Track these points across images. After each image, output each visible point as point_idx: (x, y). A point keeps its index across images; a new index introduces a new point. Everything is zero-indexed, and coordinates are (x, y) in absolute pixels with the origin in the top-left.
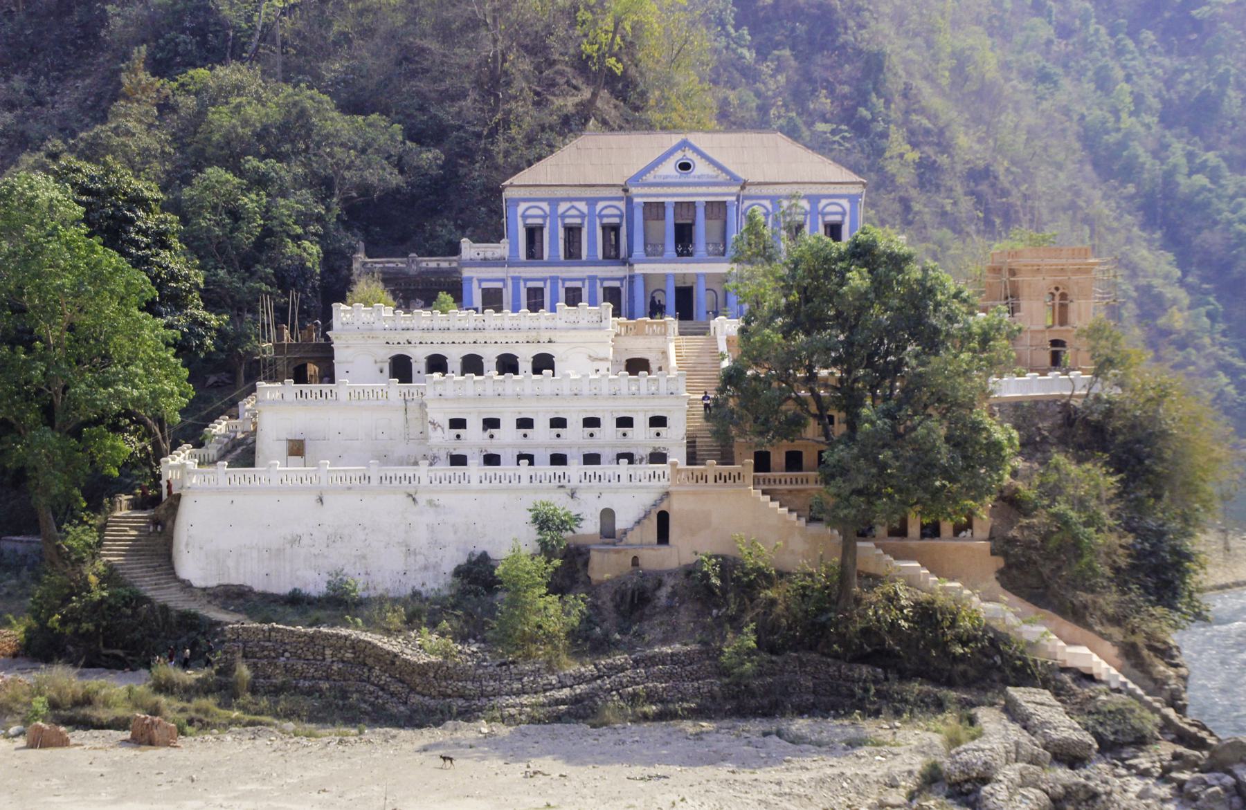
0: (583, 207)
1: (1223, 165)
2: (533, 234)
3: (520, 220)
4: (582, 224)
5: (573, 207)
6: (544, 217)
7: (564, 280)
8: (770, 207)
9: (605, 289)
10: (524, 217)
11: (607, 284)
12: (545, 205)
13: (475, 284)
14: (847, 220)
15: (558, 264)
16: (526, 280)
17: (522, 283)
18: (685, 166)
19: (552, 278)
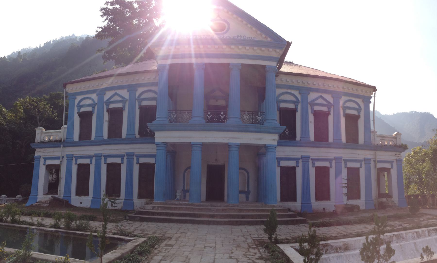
2: (86, 117)
4: (124, 107)
5: (321, 97)
6: (93, 105)
7: (314, 160)
9: (282, 168)
11: (110, 160)
13: (42, 160)
17: (103, 159)
19: (336, 159)
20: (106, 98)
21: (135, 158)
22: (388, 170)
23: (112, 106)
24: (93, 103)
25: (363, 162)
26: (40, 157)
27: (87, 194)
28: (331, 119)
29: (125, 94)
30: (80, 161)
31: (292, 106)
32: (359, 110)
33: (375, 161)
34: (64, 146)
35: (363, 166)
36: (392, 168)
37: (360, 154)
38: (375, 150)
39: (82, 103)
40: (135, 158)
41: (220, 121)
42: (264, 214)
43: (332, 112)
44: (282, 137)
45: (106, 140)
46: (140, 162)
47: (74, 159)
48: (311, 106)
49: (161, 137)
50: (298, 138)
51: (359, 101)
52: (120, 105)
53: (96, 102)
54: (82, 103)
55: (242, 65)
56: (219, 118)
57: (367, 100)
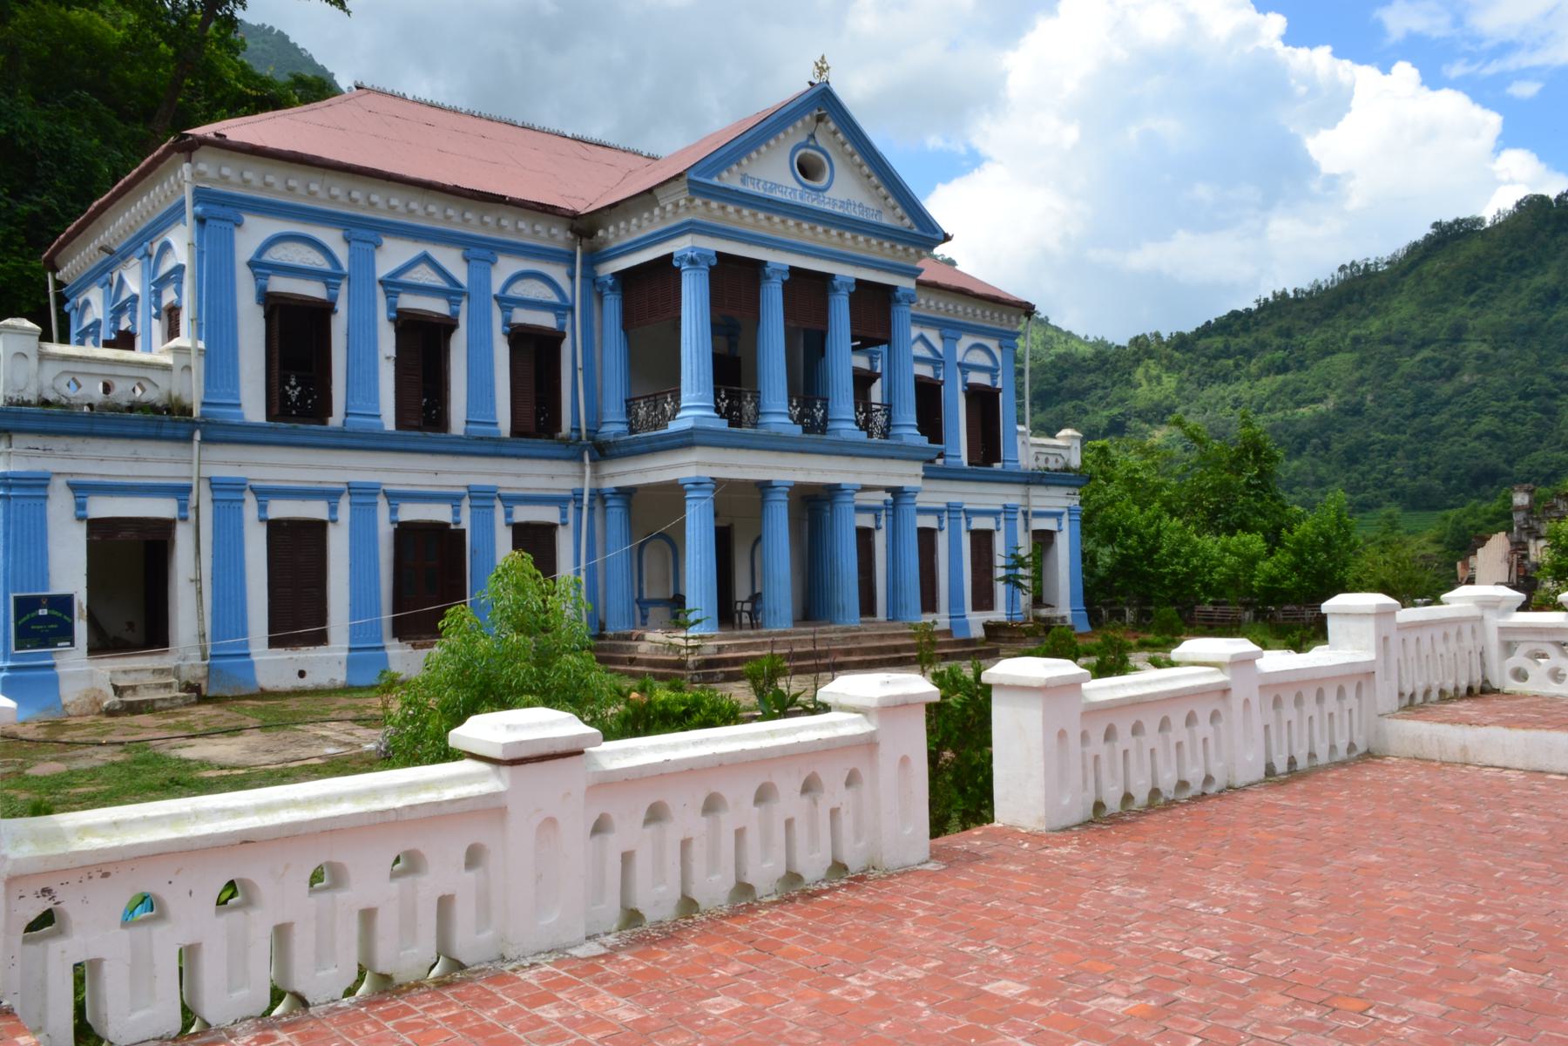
5: (426, 259)
8: (341, 252)
10: (259, 266)
12: (452, 260)
16: (396, 498)
18: (807, 170)
19: (354, 490)
24: (555, 299)
25: (466, 504)
27: (321, 639)
28: (458, 346)
30: (282, 509)
33: (1025, 514)
34: (204, 440)
38: (1027, 483)
43: (342, 306)
48: (386, 292)
50: (336, 420)
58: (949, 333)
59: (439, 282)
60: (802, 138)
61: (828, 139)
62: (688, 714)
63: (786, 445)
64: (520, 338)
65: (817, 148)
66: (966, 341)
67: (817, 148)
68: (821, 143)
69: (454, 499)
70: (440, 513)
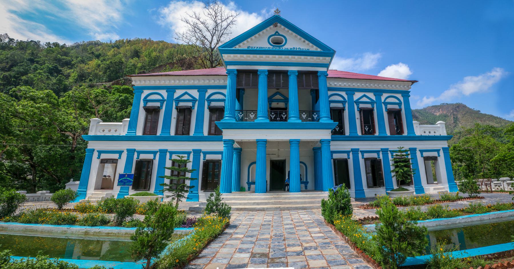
0: (195, 93)
1: (60, 68)
2: (152, 112)
3: (206, 103)
5: (365, 96)
6: (162, 101)
7: (363, 152)
8: (346, 97)
9: (366, 160)
11: (366, 155)
12: (371, 95)
13: (96, 154)
14: (403, 107)
15: (202, 139)
17: (168, 155)
18: (277, 43)
19: (353, 150)
20: (176, 96)
21: (202, 155)
22: (435, 159)
23: (181, 104)
24: (162, 99)
26: (94, 150)
28: (346, 114)
29: (195, 93)
31: (340, 105)
32: (400, 104)
35: (191, 159)
36: (439, 156)
37: (407, 145)
39: (149, 98)
40: (202, 155)
41: (282, 119)
42: (233, 167)
44: (334, 133)
45: (172, 136)
46: (172, 158)
47: (389, 153)
49: (228, 134)
51: (399, 96)
52: (190, 104)
53: (166, 98)
54: (149, 98)
55: (298, 71)
56: (313, 118)
57: (406, 94)
58: (378, 93)
59: (190, 98)
60: (273, 33)
61: (282, 30)
62: (261, 256)
63: (352, 139)
64: (390, 112)
65: (279, 35)
66: (385, 95)
67: (279, 35)
68: (281, 33)
69: (378, 152)
70: (375, 155)
